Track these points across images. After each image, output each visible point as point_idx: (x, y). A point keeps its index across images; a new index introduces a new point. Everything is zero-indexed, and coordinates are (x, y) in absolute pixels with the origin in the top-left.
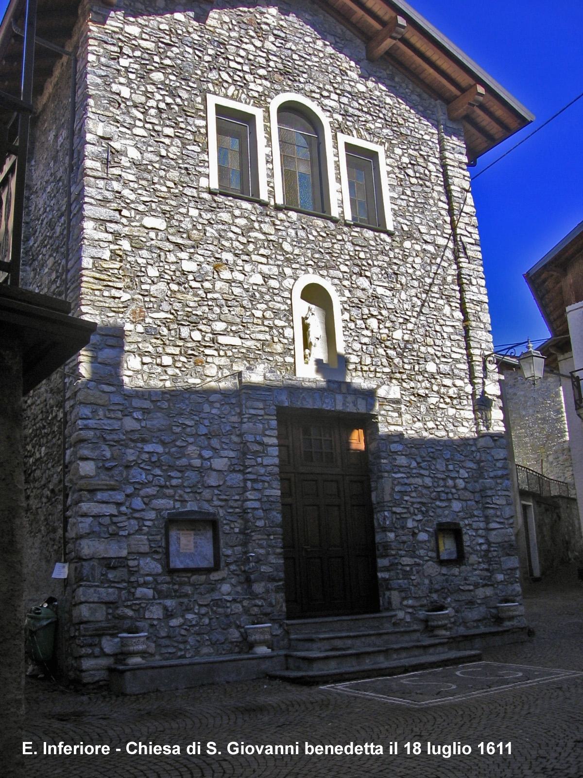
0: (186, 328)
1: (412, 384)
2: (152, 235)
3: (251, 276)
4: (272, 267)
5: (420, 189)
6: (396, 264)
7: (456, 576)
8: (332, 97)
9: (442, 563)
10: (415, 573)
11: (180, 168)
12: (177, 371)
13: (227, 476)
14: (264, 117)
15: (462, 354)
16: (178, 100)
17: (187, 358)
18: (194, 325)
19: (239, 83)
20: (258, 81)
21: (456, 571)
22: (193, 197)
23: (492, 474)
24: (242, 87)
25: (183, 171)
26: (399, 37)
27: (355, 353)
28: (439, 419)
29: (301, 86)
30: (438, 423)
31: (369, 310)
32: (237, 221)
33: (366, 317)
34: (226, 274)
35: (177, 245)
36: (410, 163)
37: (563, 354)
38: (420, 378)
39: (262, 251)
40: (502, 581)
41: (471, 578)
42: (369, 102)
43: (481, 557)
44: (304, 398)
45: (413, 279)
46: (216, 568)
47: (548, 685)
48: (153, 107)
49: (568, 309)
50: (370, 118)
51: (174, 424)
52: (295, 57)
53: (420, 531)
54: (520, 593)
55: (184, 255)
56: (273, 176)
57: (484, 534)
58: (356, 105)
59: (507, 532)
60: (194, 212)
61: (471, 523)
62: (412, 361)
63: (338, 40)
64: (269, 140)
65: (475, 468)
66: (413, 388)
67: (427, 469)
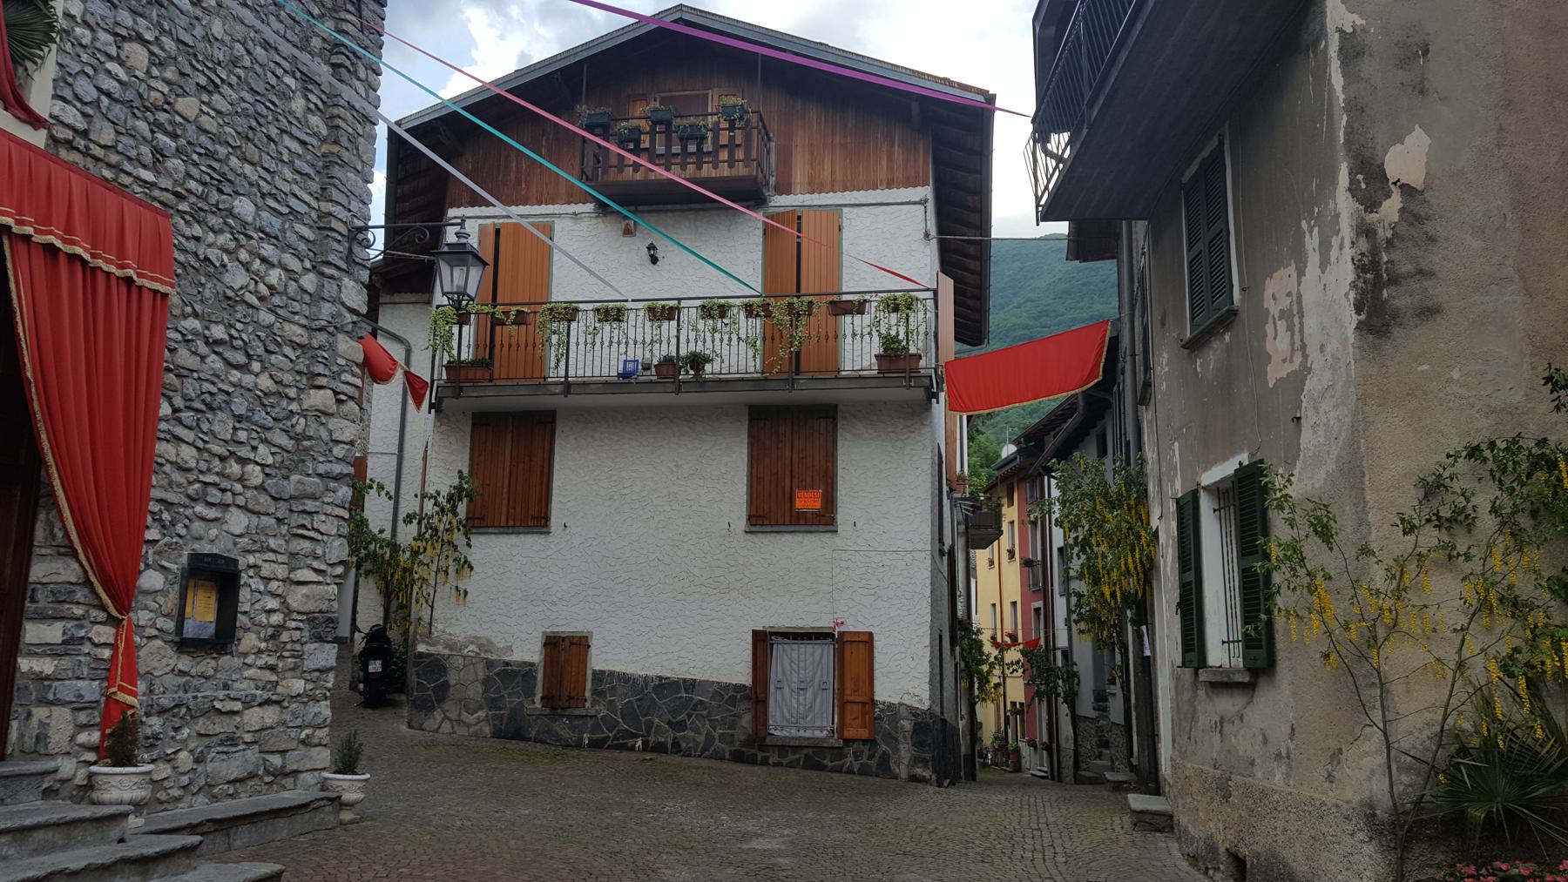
1: (197, 230)
7: (208, 678)
9: (185, 645)
15: (309, 206)
21: (207, 665)
23: (321, 469)
27: (78, 105)
28: (239, 326)
30: (233, 332)
31: (135, 22)
33: (124, 32)
37: (392, 294)
38: (214, 220)
40: (299, 695)
41: (236, 685)
43: (265, 641)
53: (148, 566)
54: (328, 721)
57: (280, 592)
59: (327, 592)
61: (259, 563)
62: (208, 178)
65: (290, 448)
67: (190, 428)
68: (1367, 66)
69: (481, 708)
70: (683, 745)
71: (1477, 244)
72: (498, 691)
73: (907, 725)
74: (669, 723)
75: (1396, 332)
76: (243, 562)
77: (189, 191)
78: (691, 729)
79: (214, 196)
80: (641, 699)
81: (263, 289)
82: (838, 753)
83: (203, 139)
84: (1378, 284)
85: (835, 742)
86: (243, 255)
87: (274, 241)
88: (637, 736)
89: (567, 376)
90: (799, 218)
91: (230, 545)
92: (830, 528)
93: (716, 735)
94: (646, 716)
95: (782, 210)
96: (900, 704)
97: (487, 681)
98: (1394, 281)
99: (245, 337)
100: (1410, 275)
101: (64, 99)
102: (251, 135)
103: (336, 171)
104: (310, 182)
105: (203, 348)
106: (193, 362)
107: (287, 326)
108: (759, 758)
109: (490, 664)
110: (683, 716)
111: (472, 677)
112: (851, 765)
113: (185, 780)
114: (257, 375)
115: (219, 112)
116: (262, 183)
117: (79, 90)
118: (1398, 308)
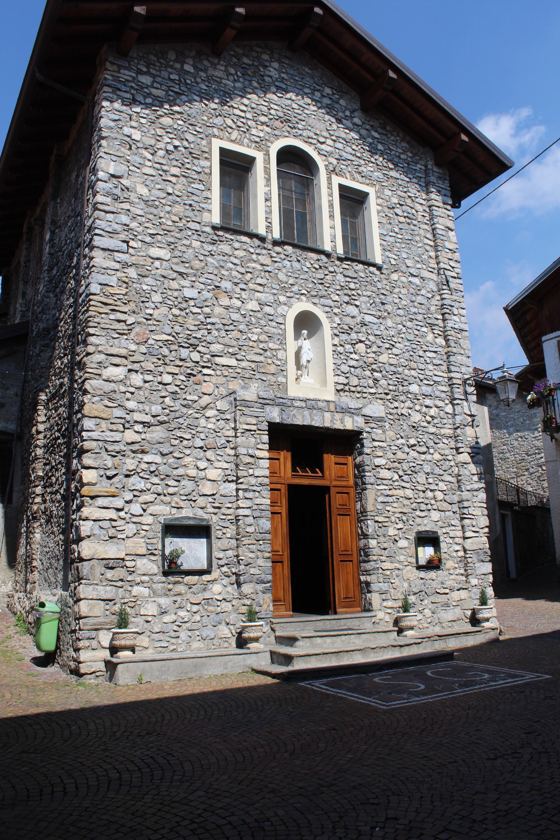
0: (186, 350)
1: (396, 404)
2: (157, 264)
3: (248, 303)
4: (268, 295)
5: (407, 226)
6: (383, 294)
10: (395, 577)
11: (184, 204)
12: (177, 389)
13: (221, 485)
14: (265, 160)
16: (185, 143)
17: (186, 377)
18: (194, 346)
19: (242, 129)
20: (260, 127)
21: (432, 574)
22: (196, 231)
24: (245, 132)
25: (187, 207)
29: (300, 132)
32: (236, 253)
34: (225, 301)
35: (181, 274)
36: (399, 204)
38: (403, 398)
39: (259, 281)
45: (399, 309)
46: (208, 572)
48: (161, 149)
50: (363, 162)
51: (172, 437)
52: (295, 106)
55: (186, 283)
56: (271, 212)
60: (196, 244)
61: (448, 531)
62: (396, 383)
63: (335, 92)
64: (268, 180)
76: (440, 532)
77: (390, 390)
79: (401, 388)
81: (429, 419)
83: (392, 368)
91: (434, 526)
99: (424, 440)
101: (338, 375)
102: (411, 358)
103: (452, 359)
104: (441, 367)
105: (407, 449)
106: (404, 456)
113: (429, 620)
114: (432, 454)
115: (396, 355)
116: (420, 376)
117: (343, 370)
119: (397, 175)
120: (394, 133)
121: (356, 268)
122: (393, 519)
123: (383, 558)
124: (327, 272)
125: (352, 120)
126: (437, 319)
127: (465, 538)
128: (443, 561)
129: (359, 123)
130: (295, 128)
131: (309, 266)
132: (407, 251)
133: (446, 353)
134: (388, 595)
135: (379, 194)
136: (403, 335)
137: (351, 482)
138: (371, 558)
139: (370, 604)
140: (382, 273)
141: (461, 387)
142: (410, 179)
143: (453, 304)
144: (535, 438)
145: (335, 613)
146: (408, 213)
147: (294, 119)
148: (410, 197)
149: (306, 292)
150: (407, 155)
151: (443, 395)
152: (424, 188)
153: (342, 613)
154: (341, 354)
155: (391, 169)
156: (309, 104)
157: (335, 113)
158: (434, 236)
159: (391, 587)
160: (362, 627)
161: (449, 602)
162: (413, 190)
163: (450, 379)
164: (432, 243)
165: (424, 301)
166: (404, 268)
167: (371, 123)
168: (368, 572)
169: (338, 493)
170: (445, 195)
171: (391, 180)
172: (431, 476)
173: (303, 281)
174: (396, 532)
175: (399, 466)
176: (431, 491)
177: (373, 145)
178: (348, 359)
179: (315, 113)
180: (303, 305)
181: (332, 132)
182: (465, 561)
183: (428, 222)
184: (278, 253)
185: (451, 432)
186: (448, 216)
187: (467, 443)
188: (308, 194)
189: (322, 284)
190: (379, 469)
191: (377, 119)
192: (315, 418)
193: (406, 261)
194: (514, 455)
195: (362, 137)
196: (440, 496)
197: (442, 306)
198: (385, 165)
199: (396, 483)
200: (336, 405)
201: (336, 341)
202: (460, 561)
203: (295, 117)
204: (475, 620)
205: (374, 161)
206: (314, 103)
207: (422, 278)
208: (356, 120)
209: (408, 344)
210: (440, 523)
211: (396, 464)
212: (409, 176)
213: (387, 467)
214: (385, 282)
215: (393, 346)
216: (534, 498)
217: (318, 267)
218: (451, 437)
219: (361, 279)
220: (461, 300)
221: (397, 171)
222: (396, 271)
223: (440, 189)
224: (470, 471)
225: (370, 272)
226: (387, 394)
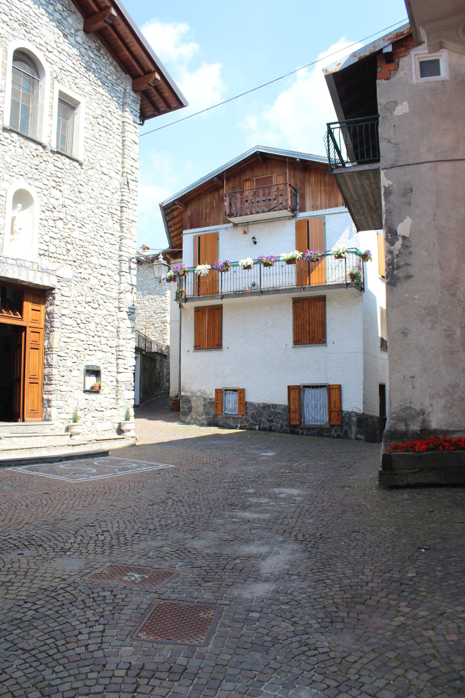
1: (80, 270)
6: (81, 185)
8: (54, 53)
10: (68, 397)
26: (110, 22)
29: (34, 38)
36: (102, 115)
37: (175, 259)
38: (86, 266)
42: (80, 63)
44: (7, 270)
47: (152, 471)
49: (184, 232)
58: (70, 63)
63: (65, 9)
66: (81, 273)
68: (393, 198)
69: (203, 415)
70: (273, 428)
71: (425, 254)
72: (208, 409)
73: (354, 419)
74: (268, 420)
75: (398, 284)
77: (77, 259)
78: (276, 422)
79: (85, 258)
80: (257, 412)
81: (103, 284)
82: (329, 430)
83: (81, 243)
84: (393, 269)
85: (328, 426)
86: (95, 274)
87: (105, 268)
88: (257, 425)
89: (222, 293)
90: (308, 221)
92: (324, 344)
93: (285, 425)
94: (259, 417)
95: (302, 218)
96: (352, 412)
97: (205, 405)
98: (398, 268)
100: (404, 266)
102: (95, 237)
103: (123, 241)
106: (82, 309)
107: (110, 293)
108: (300, 432)
109: (205, 399)
110: (272, 418)
111: (199, 404)
112: (334, 435)
115: (85, 233)
116: (100, 251)
118: (399, 277)
119: (104, 93)
120: (106, 57)
121: (64, 161)
122: (70, 355)
123: (62, 383)
124: (42, 161)
125: (75, 38)
126: (117, 210)
127: (118, 373)
128: (102, 388)
129: (81, 42)
130: (30, 33)
131: (29, 153)
132: (103, 154)
133: (120, 237)
134: (63, 409)
135: (88, 105)
136: (91, 219)
137: (42, 325)
138: (53, 382)
139: (50, 415)
140: (82, 168)
141: (127, 263)
142: (112, 97)
143: (129, 200)
144: (162, 301)
145: (23, 421)
146: (107, 124)
147: (30, 24)
148: (110, 112)
149: (24, 174)
150: (113, 78)
151: (114, 268)
152: (121, 107)
153: (29, 421)
154: (45, 226)
155: (100, 86)
156: (43, 15)
157: (63, 28)
158: (123, 146)
159: (65, 404)
160: (43, 431)
161: (104, 417)
162: (113, 106)
163: (121, 256)
164: (121, 152)
165: (109, 194)
166: (98, 167)
167: (90, 45)
168: (49, 392)
169: (32, 332)
170: (135, 116)
171: (98, 95)
172: (99, 325)
173: (23, 165)
174: (72, 364)
175: (78, 316)
176: (98, 336)
177: (89, 64)
178: (50, 231)
179: (47, 24)
180: (22, 184)
181: (59, 45)
182: (117, 389)
183: (120, 134)
184: (6, 138)
185: (117, 295)
186: (136, 132)
187: (127, 304)
188: (33, 92)
189: (37, 169)
190: (64, 317)
191: (95, 42)
192: (23, 274)
193: (101, 162)
194: (145, 312)
195: (82, 55)
196: (104, 341)
197: (121, 200)
198: (96, 82)
199: (75, 329)
200: (38, 266)
201: (43, 216)
202: (113, 389)
203: (31, 23)
204: (120, 431)
205: (87, 76)
206: (47, 15)
207: (110, 176)
208: (79, 39)
209: (94, 225)
210: (102, 361)
211: (76, 315)
212: (111, 94)
213: (70, 316)
214: (83, 175)
215: (83, 226)
216: (156, 346)
217: (35, 155)
218: (116, 299)
219: (66, 170)
220: (135, 198)
221: (103, 89)
222: (92, 168)
223: (133, 110)
224: (126, 325)
225: (74, 166)
226: (75, 262)
